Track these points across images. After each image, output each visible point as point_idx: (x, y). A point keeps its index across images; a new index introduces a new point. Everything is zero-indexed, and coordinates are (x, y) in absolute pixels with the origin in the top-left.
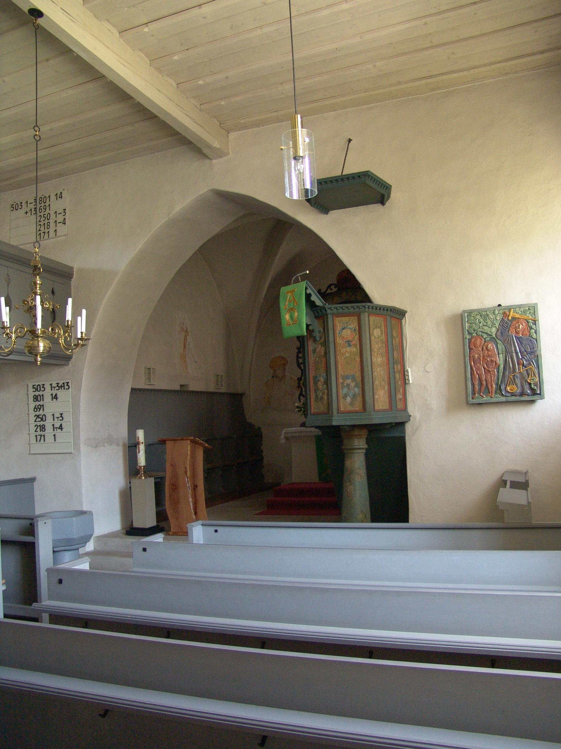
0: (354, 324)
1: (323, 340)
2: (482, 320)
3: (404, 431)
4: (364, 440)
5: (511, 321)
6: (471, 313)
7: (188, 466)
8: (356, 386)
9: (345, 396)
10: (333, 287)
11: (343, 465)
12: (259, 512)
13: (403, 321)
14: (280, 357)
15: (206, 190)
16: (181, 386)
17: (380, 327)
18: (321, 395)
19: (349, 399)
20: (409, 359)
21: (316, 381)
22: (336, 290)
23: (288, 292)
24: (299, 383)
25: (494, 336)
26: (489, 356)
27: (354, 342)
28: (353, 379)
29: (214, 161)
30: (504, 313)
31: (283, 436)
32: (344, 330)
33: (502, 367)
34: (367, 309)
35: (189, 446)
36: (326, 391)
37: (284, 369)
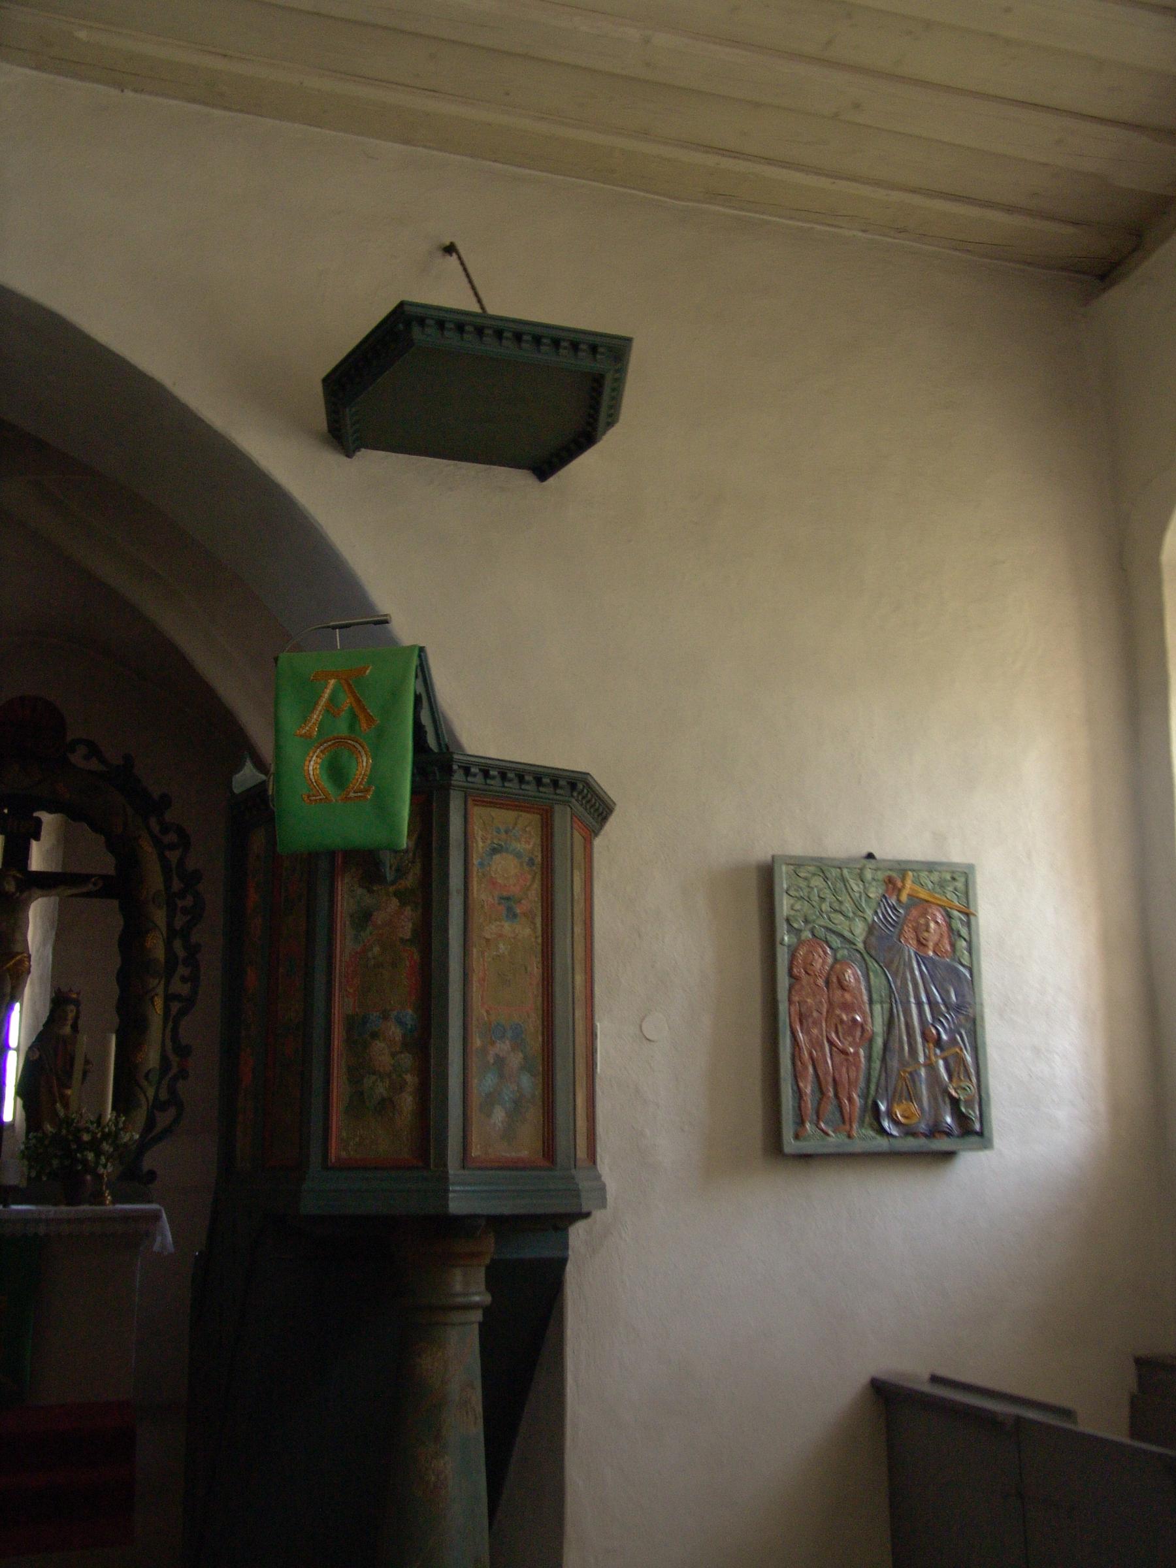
0: (528, 844)
1: (410, 880)
2: (827, 894)
3: (566, 1246)
4: (481, 1274)
5: (907, 908)
6: (799, 866)
9: (491, 1099)
18: (381, 1089)
19: (499, 1115)
21: (360, 1033)
25: (860, 946)
26: (847, 1007)
28: (518, 1043)
30: (890, 881)
32: (497, 857)
33: (879, 1041)
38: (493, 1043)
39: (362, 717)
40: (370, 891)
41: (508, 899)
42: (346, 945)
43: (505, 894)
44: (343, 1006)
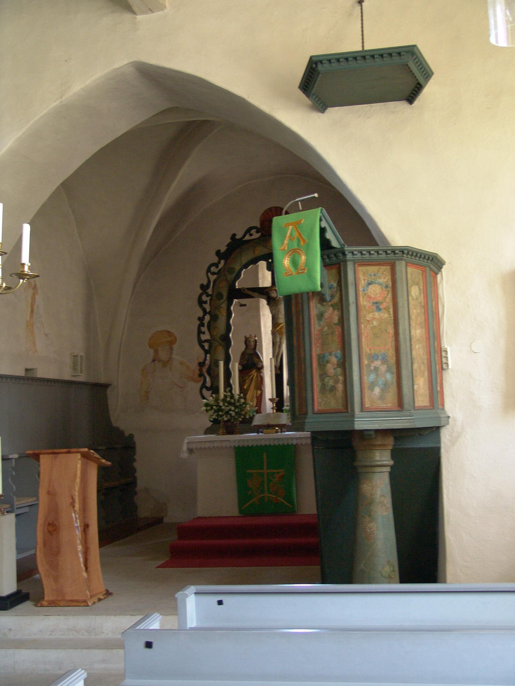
1: (336, 299)
3: (439, 441)
7: (76, 494)
8: (388, 370)
10: (253, 231)
11: (357, 490)
12: (162, 562)
13: (439, 276)
14: (163, 331)
15: (125, 62)
16: (27, 370)
17: (418, 284)
18: (331, 383)
19: (377, 390)
20: (446, 333)
21: (323, 362)
22: (259, 235)
23: (288, 225)
24: (201, 370)
27: (385, 305)
28: (384, 361)
29: (139, 17)
31: (185, 448)
32: (371, 286)
34: (405, 255)
35: (80, 462)
36: (341, 378)
37: (172, 349)
38: (373, 362)
39: (301, 240)
40: (323, 305)
41: (377, 303)
42: (316, 327)
43: (375, 301)
44: (316, 351)
